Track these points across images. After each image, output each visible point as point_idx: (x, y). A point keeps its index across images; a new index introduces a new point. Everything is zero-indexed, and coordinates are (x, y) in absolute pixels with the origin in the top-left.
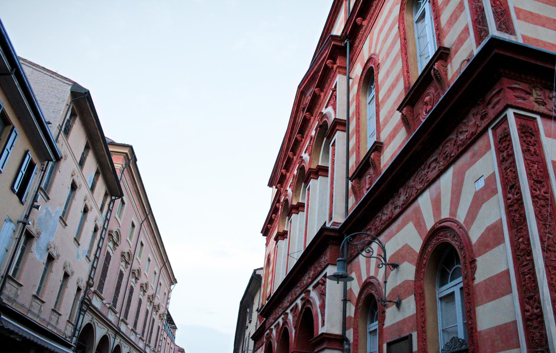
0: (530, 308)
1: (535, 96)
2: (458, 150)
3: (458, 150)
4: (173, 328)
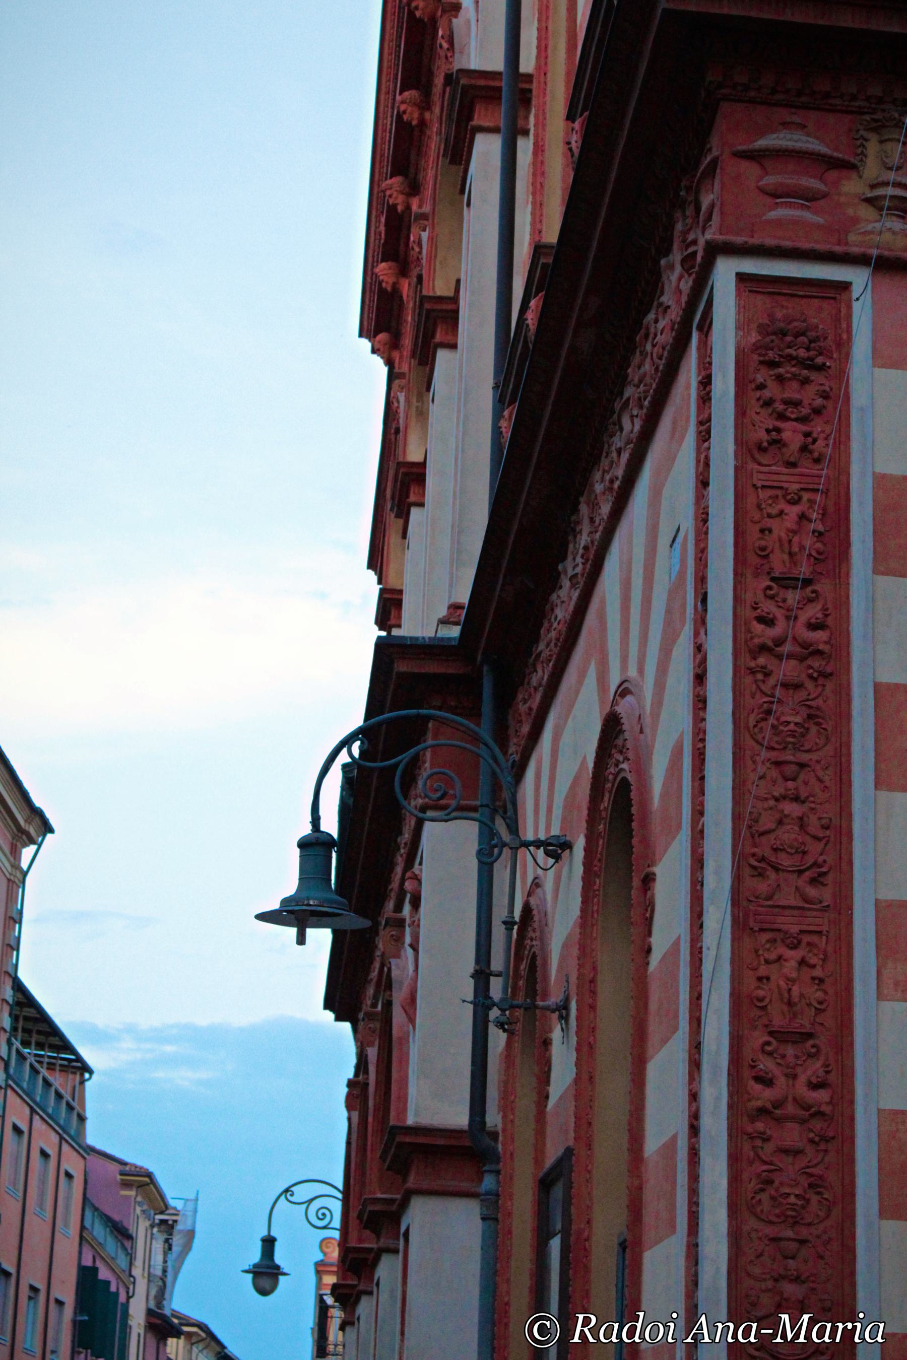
0: (777, 1071)
1: (871, 169)
2: (641, 407)
3: (641, 407)
4: (64, 1069)
